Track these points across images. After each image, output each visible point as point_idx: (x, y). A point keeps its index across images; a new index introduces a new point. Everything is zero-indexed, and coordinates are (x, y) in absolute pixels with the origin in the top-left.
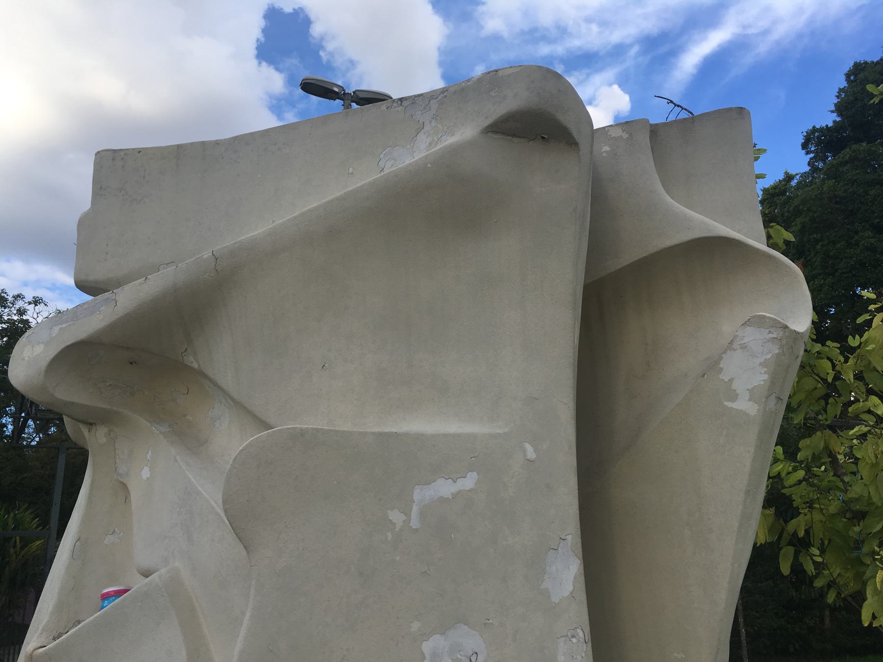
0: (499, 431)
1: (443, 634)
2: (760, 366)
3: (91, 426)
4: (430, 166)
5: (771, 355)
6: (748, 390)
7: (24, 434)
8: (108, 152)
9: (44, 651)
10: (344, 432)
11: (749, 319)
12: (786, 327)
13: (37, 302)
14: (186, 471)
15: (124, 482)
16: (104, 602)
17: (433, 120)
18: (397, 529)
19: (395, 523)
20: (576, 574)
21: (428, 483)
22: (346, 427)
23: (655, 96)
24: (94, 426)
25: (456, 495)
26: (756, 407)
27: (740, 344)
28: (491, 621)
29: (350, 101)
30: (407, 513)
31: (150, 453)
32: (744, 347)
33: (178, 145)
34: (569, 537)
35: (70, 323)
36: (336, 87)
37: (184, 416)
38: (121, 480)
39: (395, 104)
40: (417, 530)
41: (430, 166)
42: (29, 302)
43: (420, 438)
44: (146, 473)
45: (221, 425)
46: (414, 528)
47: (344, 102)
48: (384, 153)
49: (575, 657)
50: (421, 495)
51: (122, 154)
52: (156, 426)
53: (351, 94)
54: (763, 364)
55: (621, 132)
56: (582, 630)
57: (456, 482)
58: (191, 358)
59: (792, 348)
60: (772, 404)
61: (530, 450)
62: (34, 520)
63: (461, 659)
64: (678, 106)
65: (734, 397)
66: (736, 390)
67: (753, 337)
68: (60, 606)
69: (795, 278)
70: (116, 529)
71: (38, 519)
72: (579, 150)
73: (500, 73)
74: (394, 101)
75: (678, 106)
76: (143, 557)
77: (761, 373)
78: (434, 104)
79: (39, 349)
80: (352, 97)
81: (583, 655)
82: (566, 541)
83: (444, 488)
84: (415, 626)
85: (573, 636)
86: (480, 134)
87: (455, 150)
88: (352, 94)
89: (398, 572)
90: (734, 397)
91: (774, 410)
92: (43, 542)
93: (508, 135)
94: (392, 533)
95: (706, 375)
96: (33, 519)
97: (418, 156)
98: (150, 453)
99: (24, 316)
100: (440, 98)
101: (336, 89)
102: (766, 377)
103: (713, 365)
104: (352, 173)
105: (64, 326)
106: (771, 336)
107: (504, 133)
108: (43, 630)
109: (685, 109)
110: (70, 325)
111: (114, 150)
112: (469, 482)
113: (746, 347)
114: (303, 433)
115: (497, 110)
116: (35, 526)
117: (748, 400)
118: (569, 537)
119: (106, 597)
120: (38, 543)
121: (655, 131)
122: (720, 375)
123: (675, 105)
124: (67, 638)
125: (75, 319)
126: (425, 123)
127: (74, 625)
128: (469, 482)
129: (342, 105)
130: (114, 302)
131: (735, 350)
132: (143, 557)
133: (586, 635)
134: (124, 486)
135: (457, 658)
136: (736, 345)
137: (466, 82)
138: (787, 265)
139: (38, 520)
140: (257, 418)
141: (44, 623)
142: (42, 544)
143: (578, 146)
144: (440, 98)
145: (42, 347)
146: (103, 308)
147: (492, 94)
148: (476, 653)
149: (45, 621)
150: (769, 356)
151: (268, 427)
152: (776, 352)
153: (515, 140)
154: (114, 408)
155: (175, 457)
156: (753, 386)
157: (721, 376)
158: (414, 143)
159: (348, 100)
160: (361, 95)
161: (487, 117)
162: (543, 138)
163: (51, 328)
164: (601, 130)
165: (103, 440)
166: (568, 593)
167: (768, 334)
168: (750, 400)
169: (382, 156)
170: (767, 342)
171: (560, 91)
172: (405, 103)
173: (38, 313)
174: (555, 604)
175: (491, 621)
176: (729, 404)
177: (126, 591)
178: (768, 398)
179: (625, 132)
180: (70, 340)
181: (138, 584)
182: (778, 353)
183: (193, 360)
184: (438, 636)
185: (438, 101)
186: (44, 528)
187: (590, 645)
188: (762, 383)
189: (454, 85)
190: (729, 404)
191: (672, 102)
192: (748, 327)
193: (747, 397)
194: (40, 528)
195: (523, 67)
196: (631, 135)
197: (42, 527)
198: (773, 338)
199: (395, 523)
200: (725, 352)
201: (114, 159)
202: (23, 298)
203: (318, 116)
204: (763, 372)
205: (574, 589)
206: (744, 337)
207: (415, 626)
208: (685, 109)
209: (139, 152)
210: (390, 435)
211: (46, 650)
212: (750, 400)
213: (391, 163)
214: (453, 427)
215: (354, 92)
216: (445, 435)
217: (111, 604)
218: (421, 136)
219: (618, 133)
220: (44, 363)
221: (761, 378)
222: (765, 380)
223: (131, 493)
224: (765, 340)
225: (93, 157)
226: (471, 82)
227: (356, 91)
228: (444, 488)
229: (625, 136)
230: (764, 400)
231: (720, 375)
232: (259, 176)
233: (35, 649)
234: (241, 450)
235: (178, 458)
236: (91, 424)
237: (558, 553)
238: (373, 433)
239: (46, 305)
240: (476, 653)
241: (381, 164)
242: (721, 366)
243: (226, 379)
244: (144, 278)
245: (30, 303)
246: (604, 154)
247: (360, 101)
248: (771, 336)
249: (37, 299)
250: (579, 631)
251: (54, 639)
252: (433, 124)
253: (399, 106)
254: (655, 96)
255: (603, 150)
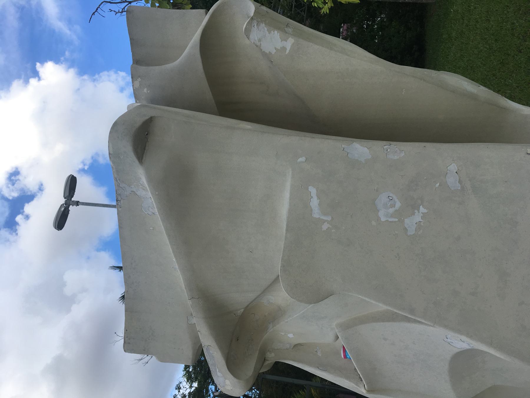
0: (291, 173)
1: (378, 211)
2: (270, 34)
3: (266, 360)
4: (157, 192)
5: (265, 28)
6: (281, 41)
7: (252, 397)
8: (125, 346)
9: (366, 385)
10: (284, 247)
11: (246, 36)
12: (252, 18)
13: (179, 387)
14: (293, 317)
15: (293, 346)
16: (347, 357)
17: (131, 186)
18: (331, 227)
19: (328, 227)
20: (360, 145)
21: (312, 210)
22: (282, 245)
23: (89, 22)
24: (265, 358)
25: (318, 197)
26: (290, 39)
27: (258, 42)
28: (376, 188)
29: (71, 201)
30: (324, 221)
31: (282, 333)
32: (260, 40)
33: (125, 311)
34: (343, 146)
35: (216, 367)
36: (61, 209)
37: (265, 316)
38: (292, 347)
39: (119, 204)
40: (332, 218)
41: (157, 192)
42: (178, 392)
43: (290, 211)
44: (291, 336)
45: (272, 300)
46: (331, 219)
47: (71, 205)
48: (144, 212)
49: (396, 151)
50: (316, 214)
51: (126, 339)
52: (269, 329)
53: (66, 200)
54: (270, 33)
55: (137, 81)
56: (385, 146)
57: (312, 197)
58: (239, 312)
59: (262, 15)
60: (290, 30)
61: (302, 159)
62: (300, 393)
63: (390, 204)
64: (97, 9)
65: (284, 49)
66: (281, 47)
67: (256, 34)
68: (348, 378)
69: (225, 3)
70: (315, 350)
71: (300, 391)
72: (154, 116)
73: (111, 152)
74: (117, 204)
75: (97, 9)
76: (329, 338)
77: (274, 34)
78: (122, 185)
79: (228, 382)
80: (68, 200)
81: (396, 147)
82: (345, 148)
83: (315, 203)
84: (374, 223)
85: (387, 150)
86: (142, 166)
87: (150, 180)
88: (66, 199)
89: (349, 228)
90: (284, 49)
91: (293, 29)
92: (312, 388)
93: (144, 152)
94: (332, 229)
95: (272, 61)
96: (300, 393)
97: (150, 195)
98: (282, 333)
99: (186, 395)
100: (119, 182)
101: (63, 209)
102: (276, 32)
103: (267, 56)
104: (153, 228)
105: (218, 370)
106: (255, 26)
107: (143, 154)
108: (357, 385)
109: (100, 6)
110: (217, 367)
111: (124, 343)
112: (313, 190)
113: (260, 39)
114: (283, 266)
115: (132, 157)
116: (303, 392)
117: (287, 42)
118: (343, 146)
119: (345, 357)
120: (313, 391)
121: (137, 61)
122: (273, 54)
123: (96, 11)
124: (361, 375)
125: (215, 365)
126: (132, 190)
127: (357, 371)
128: (313, 190)
129: (73, 206)
130: (209, 347)
131: (261, 44)
132: (329, 338)
133: (387, 144)
134: (295, 346)
135: (390, 206)
136: (258, 44)
137: (113, 169)
138: (218, 6)
139: (300, 390)
140: (271, 284)
141: (354, 385)
142: (314, 390)
143: (153, 117)
144: (119, 182)
145: (227, 381)
146: (211, 352)
147: (122, 157)
148: (389, 197)
149: (353, 384)
150: (266, 29)
151: (277, 279)
152: (264, 25)
153: (147, 148)
154: (259, 348)
155: (285, 322)
156: (280, 39)
157: (273, 53)
158: (142, 197)
159: (70, 202)
160: (67, 194)
161: (134, 162)
162: (147, 134)
163: (218, 376)
164: (135, 91)
165: (273, 355)
166: (368, 150)
167: (254, 27)
168: (286, 41)
169: (146, 213)
170: (259, 29)
171: (123, 124)
172: (119, 199)
173: (184, 388)
174: (371, 157)
175: (376, 188)
176: (287, 51)
177: (344, 347)
178: (286, 32)
179: (137, 79)
180: (225, 368)
181: (341, 342)
182: (265, 24)
183: (239, 311)
184: (379, 213)
185: (121, 183)
186: (305, 388)
187: (391, 143)
188: (279, 34)
189: (114, 174)
190: (287, 51)
191: (94, 13)
192: (250, 36)
193: (285, 42)
194: (305, 390)
195: (110, 141)
196: (139, 76)
197: (305, 389)
198: (257, 25)
199: (328, 227)
200: (261, 50)
201: (129, 343)
202: (176, 395)
203: (120, 242)
204: (273, 33)
205: (367, 147)
206: (255, 39)
207: (374, 223)
208: (100, 6)
209: (127, 330)
210: (287, 225)
211: (366, 384)
212: (286, 41)
213: (151, 209)
214: (287, 195)
215: (65, 198)
216: (290, 199)
217: (349, 355)
218: (138, 193)
219: (137, 84)
220: (235, 380)
221: (276, 34)
222: (277, 32)
223: (298, 343)
224: (258, 29)
225: (127, 353)
226: (114, 166)
227: (64, 197)
228: (315, 203)
229: (139, 79)
230: (287, 34)
231: (273, 54)
232: (148, 273)
233: (365, 389)
234: (288, 294)
235: (286, 321)
236: (265, 359)
237: (349, 152)
238: (286, 233)
239: (181, 383)
240: (389, 197)
241: (150, 213)
242: (268, 53)
243: (251, 296)
244: (198, 332)
245: (179, 391)
246: (149, 92)
247: (71, 195)
248: (255, 26)
249: (177, 387)
250: (385, 147)
251: (362, 380)
252: (133, 186)
253: (121, 202)
254: (89, 22)
255: (146, 92)
